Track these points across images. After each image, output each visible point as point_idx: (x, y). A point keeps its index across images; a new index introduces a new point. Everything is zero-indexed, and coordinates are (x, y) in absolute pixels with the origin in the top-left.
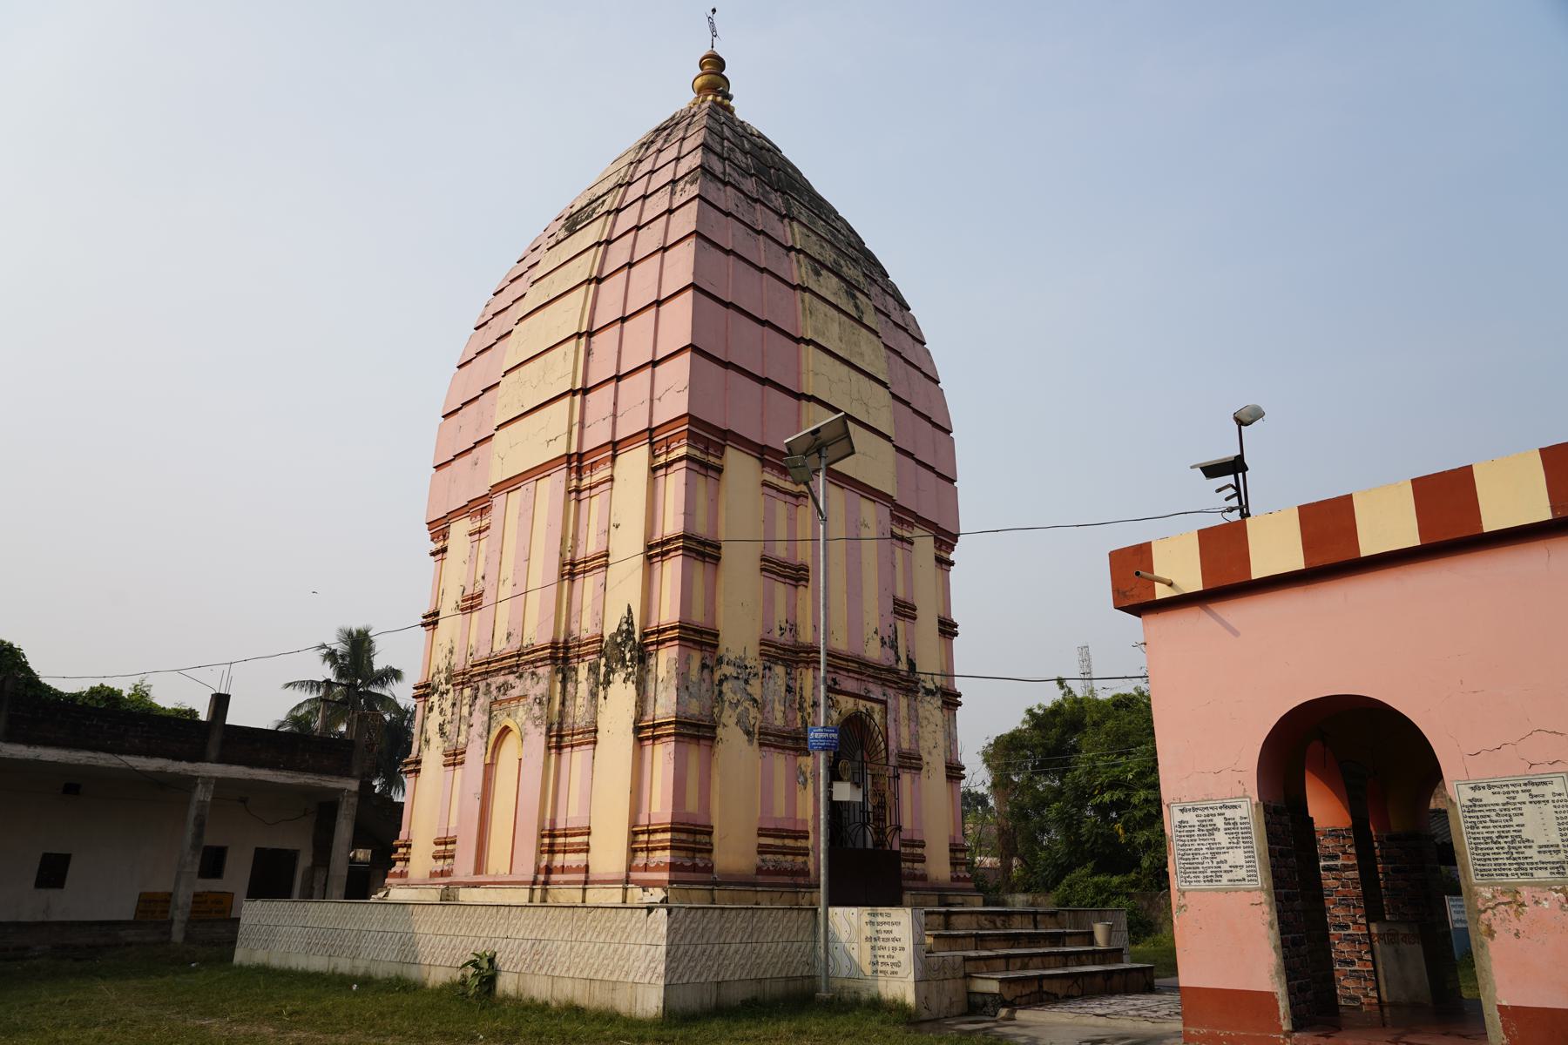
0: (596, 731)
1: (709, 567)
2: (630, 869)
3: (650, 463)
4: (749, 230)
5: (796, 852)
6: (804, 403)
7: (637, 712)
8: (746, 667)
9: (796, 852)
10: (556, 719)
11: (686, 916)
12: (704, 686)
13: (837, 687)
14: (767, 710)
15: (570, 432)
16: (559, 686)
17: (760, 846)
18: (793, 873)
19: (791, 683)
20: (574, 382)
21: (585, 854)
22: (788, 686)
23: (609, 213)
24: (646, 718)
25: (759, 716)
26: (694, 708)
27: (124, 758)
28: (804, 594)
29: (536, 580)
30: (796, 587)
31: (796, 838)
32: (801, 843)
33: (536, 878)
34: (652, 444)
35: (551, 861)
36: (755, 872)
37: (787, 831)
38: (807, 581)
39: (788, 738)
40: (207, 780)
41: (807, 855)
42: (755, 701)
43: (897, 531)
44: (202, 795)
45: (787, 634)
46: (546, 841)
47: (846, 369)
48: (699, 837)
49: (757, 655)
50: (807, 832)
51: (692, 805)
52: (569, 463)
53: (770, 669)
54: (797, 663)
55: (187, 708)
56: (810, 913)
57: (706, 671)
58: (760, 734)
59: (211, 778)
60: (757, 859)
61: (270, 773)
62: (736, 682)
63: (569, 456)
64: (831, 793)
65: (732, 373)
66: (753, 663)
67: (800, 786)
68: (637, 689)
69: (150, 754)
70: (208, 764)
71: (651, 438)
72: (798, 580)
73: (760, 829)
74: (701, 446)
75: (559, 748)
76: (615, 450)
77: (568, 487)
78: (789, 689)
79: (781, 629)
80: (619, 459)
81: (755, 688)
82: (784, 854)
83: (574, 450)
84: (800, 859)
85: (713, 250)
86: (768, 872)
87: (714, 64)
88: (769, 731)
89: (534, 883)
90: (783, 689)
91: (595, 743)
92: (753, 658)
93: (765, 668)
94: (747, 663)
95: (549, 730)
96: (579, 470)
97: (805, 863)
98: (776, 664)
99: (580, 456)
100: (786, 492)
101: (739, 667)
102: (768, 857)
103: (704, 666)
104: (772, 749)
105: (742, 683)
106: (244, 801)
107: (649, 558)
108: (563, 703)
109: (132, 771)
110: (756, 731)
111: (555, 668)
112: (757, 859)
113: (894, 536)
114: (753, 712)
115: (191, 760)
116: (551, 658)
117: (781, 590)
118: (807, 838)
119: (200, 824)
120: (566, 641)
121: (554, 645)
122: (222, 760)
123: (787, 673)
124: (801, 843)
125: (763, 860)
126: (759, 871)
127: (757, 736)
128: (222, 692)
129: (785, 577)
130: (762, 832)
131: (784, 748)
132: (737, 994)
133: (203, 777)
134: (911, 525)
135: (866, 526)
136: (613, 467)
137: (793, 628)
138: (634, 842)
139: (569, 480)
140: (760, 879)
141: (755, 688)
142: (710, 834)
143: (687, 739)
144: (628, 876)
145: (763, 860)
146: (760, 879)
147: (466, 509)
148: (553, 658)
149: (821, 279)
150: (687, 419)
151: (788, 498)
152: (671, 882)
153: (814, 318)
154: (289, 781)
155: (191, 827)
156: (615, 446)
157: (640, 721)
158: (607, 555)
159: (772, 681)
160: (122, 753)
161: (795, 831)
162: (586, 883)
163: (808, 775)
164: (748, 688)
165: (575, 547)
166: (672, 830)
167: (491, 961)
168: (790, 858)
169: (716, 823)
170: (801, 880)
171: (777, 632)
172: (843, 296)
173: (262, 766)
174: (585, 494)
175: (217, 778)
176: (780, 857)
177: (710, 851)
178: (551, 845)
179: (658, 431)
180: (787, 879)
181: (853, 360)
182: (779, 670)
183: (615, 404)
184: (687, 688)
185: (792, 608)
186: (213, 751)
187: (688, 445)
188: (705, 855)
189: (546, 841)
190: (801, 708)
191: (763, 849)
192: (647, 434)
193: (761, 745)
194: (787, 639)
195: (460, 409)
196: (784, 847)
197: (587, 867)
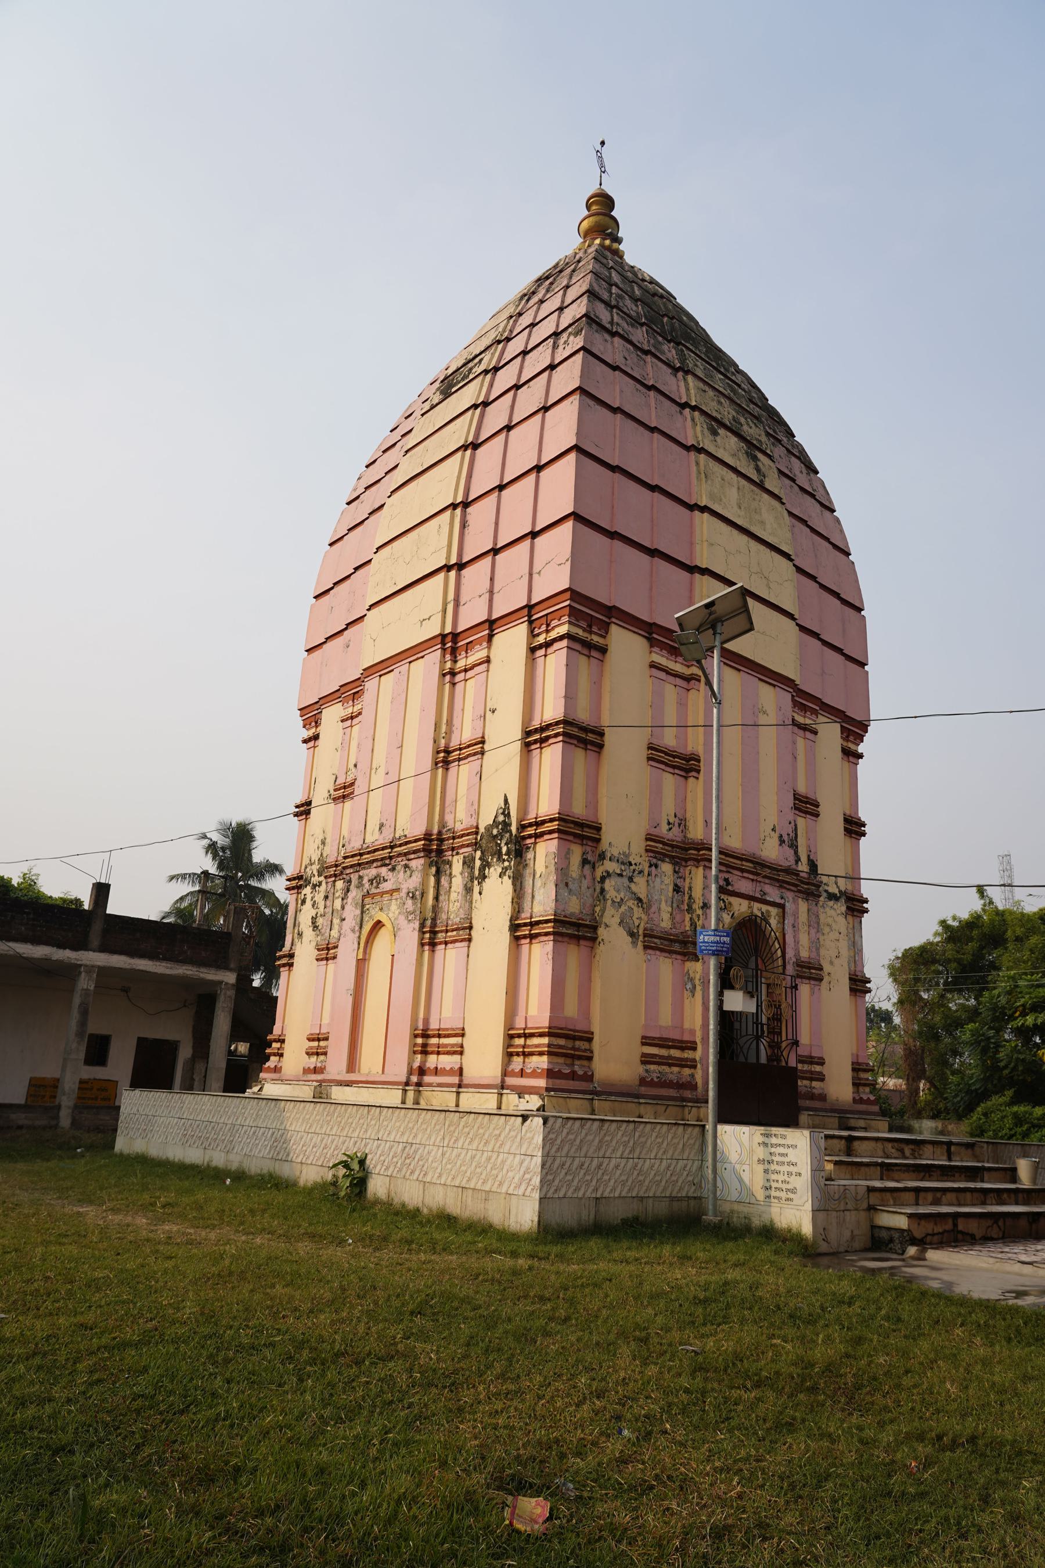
0: (471, 928)
1: (592, 755)
2: (505, 1073)
3: (529, 643)
4: (638, 386)
5: (682, 1063)
6: (697, 576)
7: (513, 909)
8: (631, 864)
9: (682, 1063)
10: (429, 914)
11: (563, 1126)
12: (585, 883)
13: (730, 888)
14: (653, 910)
15: (444, 611)
16: (432, 880)
17: (644, 1055)
18: (680, 1086)
19: (679, 882)
20: (448, 557)
21: (459, 1057)
22: (676, 885)
23: (486, 372)
24: (523, 915)
25: (643, 916)
26: (574, 907)
27: (11, 944)
28: (695, 786)
29: (409, 768)
30: (686, 778)
31: (682, 1049)
32: (688, 1054)
33: (408, 1078)
34: (531, 622)
35: (424, 1062)
36: (637, 1082)
37: (673, 1040)
38: (698, 771)
39: (675, 941)
40: (90, 969)
41: (695, 1067)
42: (640, 900)
43: (800, 719)
44: (85, 983)
45: (676, 830)
46: (419, 1041)
47: (745, 538)
48: (578, 1043)
49: (643, 852)
50: (695, 1043)
51: (571, 1010)
52: (443, 643)
53: (656, 866)
54: (686, 860)
55: (73, 897)
56: (697, 1129)
57: (587, 867)
58: (645, 936)
59: (93, 966)
60: (641, 1069)
61: (150, 963)
62: (620, 879)
63: (443, 637)
64: (722, 1002)
65: (618, 544)
66: (638, 860)
67: (687, 994)
68: (514, 884)
69: (36, 941)
70: (91, 953)
71: (530, 616)
72: (687, 771)
73: (643, 1037)
74: (584, 624)
75: (433, 945)
76: (491, 630)
77: (442, 669)
78: (677, 889)
79: (669, 823)
80: (496, 639)
81: (640, 886)
82: (670, 1065)
83: (448, 630)
84: (687, 1071)
85: (598, 408)
86: (652, 1084)
87: (603, 203)
88: (655, 933)
89: (407, 1084)
90: (671, 888)
91: (470, 940)
92: (638, 854)
93: (651, 866)
94: (631, 859)
95: (422, 925)
96: (454, 651)
97: (692, 1076)
98: (663, 861)
99: (455, 636)
100: (676, 675)
101: (623, 863)
102: (652, 1067)
103: (585, 862)
104: (658, 953)
105: (625, 880)
106: (125, 990)
107: (527, 745)
108: (437, 898)
109: (19, 957)
110: (641, 932)
111: (428, 861)
112: (641, 1069)
113: (795, 723)
114: (638, 912)
115: (75, 948)
116: (424, 850)
117: (669, 781)
118: (695, 1049)
119: (84, 1012)
120: (440, 833)
121: (427, 837)
122: (103, 949)
123: (675, 871)
124: (688, 1054)
125: (647, 1071)
126: (643, 1081)
127: (641, 938)
128: (103, 881)
129: (674, 767)
130: (646, 1041)
131: (670, 952)
132: (617, 1213)
133: (86, 966)
134: (815, 712)
135: (764, 713)
136: (489, 647)
137: (683, 823)
138: (510, 1046)
139: (443, 662)
140: (643, 1090)
141: (640, 886)
142: (590, 1040)
143: (566, 939)
144: (503, 1081)
145: (647, 1071)
146: (643, 1090)
147: (338, 694)
148: (427, 851)
149: (718, 438)
150: (568, 595)
151: (679, 681)
152: (548, 1089)
153: (709, 482)
154: (168, 972)
155: (75, 1014)
156: (491, 625)
157: (517, 919)
158: (483, 742)
159: (658, 880)
160: (9, 940)
161: (682, 1042)
162: (460, 1086)
163: (697, 982)
164: (632, 886)
165: (449, 733)
166: (549, 1034)
167: (362, 1162)
168: (676, 1069)
169: (596, 1028)
170: (688, 1094)
171: (665, 827)
172: (742, 456)
173: (142, 956)
174: (459, 677)
175: (99, 967)
176: (666, 1069)
177: (590, 1059)
178: (425, 1045)
179: (498, 623)
180: (672, 1093)
181: (753, 529)
182: (667, 868)
183: (492, 579)
184: (567, 884)
185: (682, 800)
186: (95, 940)
187: (570, 623)
188: (585, 1063)
189: (419, 1041)
190: (690, 910)
191: (646, 1060)
192: (525, 612)
193: (646, 947)
194: (675, 834)
195: (332, 588)
196: (670, 1057)
197: (461, 1069)
